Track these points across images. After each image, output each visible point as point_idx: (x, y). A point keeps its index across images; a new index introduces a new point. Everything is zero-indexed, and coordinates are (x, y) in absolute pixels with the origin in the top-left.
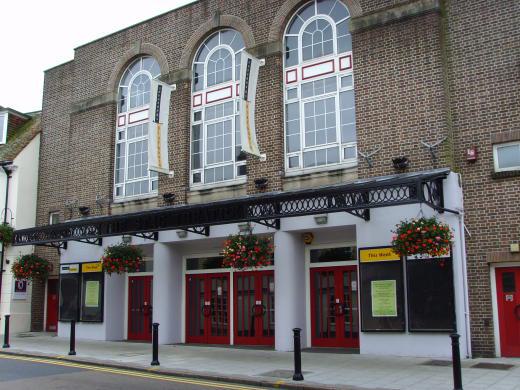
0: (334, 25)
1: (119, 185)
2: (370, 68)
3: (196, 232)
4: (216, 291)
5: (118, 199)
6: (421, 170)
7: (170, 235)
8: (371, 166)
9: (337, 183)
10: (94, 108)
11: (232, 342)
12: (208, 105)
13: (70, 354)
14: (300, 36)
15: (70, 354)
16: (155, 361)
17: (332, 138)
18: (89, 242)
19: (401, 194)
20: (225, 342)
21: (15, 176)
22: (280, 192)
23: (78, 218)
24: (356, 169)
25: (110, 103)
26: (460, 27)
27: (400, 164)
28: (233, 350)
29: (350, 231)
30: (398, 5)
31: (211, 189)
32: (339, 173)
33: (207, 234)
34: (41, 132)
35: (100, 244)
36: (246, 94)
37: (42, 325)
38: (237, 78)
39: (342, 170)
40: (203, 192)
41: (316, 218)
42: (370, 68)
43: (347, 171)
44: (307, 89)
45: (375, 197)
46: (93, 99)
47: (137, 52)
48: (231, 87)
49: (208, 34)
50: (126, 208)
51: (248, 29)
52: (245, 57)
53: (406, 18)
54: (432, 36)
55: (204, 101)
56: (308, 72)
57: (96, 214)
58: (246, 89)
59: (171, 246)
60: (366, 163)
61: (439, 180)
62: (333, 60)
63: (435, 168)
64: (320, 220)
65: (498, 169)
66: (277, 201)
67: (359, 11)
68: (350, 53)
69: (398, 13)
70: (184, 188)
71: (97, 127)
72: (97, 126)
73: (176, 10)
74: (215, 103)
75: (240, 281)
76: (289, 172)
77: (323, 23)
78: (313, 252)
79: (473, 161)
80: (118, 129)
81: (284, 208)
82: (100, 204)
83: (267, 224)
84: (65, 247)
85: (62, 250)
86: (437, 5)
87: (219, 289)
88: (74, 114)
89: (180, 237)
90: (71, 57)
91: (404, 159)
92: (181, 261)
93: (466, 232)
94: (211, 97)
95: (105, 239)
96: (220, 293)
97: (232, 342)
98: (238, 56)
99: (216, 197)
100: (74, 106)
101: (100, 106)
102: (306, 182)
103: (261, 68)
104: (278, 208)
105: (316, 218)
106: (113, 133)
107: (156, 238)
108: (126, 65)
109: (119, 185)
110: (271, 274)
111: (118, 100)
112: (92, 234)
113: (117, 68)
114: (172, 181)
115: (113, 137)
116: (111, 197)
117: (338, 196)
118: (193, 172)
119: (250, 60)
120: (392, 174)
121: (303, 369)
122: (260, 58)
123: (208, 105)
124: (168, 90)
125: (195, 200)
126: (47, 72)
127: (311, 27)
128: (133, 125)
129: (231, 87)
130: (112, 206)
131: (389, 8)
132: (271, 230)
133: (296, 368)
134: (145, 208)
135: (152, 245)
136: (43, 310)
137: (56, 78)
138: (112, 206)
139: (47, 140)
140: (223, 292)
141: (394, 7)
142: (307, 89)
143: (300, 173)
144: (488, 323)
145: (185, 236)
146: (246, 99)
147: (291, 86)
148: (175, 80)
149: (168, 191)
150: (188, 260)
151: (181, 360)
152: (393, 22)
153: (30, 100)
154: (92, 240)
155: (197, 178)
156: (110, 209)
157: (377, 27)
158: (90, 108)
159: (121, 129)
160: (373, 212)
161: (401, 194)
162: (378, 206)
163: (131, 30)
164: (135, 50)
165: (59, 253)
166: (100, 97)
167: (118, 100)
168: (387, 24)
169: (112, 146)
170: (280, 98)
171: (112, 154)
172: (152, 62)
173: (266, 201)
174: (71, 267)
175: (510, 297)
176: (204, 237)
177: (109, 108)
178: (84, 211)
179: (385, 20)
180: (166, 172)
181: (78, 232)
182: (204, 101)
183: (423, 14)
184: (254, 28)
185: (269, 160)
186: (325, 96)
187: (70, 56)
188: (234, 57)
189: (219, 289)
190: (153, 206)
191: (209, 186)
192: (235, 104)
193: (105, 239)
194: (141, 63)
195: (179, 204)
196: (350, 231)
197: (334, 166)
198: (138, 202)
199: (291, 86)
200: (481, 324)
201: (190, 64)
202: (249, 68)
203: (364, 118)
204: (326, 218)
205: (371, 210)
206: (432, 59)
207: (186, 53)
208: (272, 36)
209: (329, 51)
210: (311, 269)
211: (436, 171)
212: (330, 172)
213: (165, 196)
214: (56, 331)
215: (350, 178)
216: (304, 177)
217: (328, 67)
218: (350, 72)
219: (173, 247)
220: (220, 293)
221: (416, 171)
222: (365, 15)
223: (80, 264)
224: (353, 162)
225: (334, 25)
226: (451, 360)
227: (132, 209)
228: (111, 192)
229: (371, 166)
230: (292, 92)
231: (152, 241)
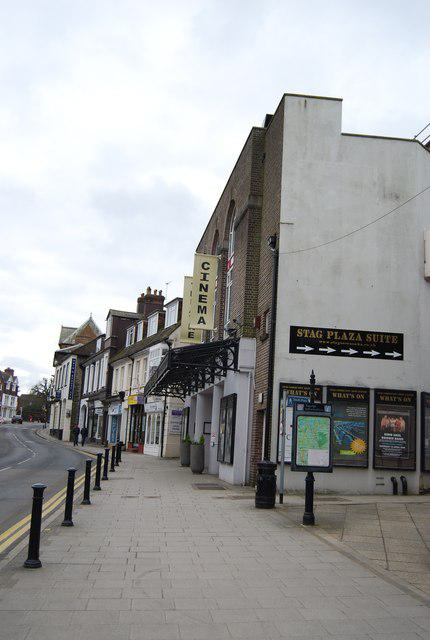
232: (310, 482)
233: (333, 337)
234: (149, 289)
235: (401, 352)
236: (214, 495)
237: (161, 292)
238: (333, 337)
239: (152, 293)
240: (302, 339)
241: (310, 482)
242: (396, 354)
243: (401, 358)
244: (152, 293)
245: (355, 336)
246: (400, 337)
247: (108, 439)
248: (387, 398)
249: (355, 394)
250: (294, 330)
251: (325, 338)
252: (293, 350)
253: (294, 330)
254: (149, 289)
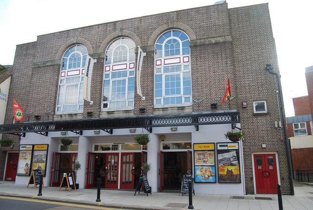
0: (181, 42)
2: (199, 63)
4: (111, 162)
5: (57, 113)
7: (90, 133)
10: (48, 66)
11: (119, 188)
12: (113, 71)
13: (39, 195)
14: (68, 58)
15: (39, 195)
16: (40, 194)
17: (179, 92)
18: (41, 134)
19: (189, 121)
20: (115, 187)
22: (152, 115)
24: (191, 107)
25: (57, 65)
28: (119, 191)
29: (189, 135)
30: (214, 37)
31: (130, 110)
32: (183, 108)
33: (112, 133)
34: (12, 75)
35: (47, 135)
36: (87, 74)
37: (3, 177)
38: (84, 65)
39: (184, 107)
40: (109, 113)
41: (95, 132)
42: (199, 63)
44: (114, 75)
45: (154, 122)
46: (47, 62)
49: (115, 38)
52: (88, 57)
53: (217, 43)
54: (228, 52)
55: (111, 70)
56: (167, 62)
57: (44, 120)
58: (88, 72)
60: (196, 105)
62: (126, 64)
63: (230, 109)
64: (173, 129)
66: (151, 119)
67: (194, 37)
68: (189, 55)
69: (213, 41)
70: (99, 110)
71: (48, 76)
72: (49, 75)
73: (98, 25)
74: (71, 77)
75: (124, 157)
76: (156, 106)
77: (175, 41)
79: (245, 108)
80: (60, 78)
81: (50, 128)
82: (48, 115)
83: (76, 133)
84: (24, 136)
85: (22, 137)
86: (231, 40)
87: (113, 161)
88: (35, 68)
90: (35, 39)
91: (216, 104)
92: (58, 145)
94: (70, 74)
95: (114, 130)
96: (113, 163)
97: (119, 188)
98: (84, 59)
99: (116, 116)
100: (35, 64)
101: (50, 66)
102: (166, 112)
103: (95, 63)
104: (48, 127)
105: (95, 132)
106: (58, 80)
107: (81, 134)
111: (61, 64)
112: (43, 130)
113: (62, 48)
114: (92, 106)
116: (54, 111)
117: (180, 116)
118: (103, 103)
119: (90, 59)
121: (193, 204)
122: (94, 59)
123: (113, 71)
124: (93, 61)
125: (104, 116)
127: (169, 41)
128: (115, 71)
130: (54, 116)
131: (208, 38)
132: (78, 135)
133: (98, 197)
134: (74, 118)
135: (78, 137)
136: (4, 169)
137: (23, 50)
138: (54, 116)
139: (15, 80)
140: (115, 162)
141: (211, 38)
142: (114, 75)
143: (162, 107)
144: (252, 179)
146: (87, 76)
147: (107, 73)
149: (142, 107)
151: (89, 196)
152: (211, 44)
153: (7, 59)
154: (43, 133)
155: (105, 106)
157: (203, 45)
158: (45, 66)
159: (62, 78)
160: (200, 126)
161: (189, 121)
162: (204, 124)
163: (97, 27)
166: (52, 61)
167: (61, 64)
168: (208, 45)
169: (57, 86)
170: (153, 72)
174: (27, 146)
175: (260, 167)
176: (109, 134)
177: (56, 67)
178: (37, 117)
179: (207, 43)
180: (90, 101)
182: (111, 70)
183: (224, 43)
184: (86, 46)
185: (146, 100)
186: (122, 78)
188: (82, 57)
189: (113, 161)
190: (80, 118)
191: (166, 106)
192: (81, 78)
193: (114, 130)
194: (76, 47)
195: (95, 118)
196: (189, 135)
197: (179, 105)
198: (71, 115)
199: (159, 67)
200: (249, 179)
202: (89, 63)
203: (196, 84)
204: (135, 130)
205: (199, 126)
206: (229, 62)
208: (150, 43)
209: (178, 52)
213: (88, 113)
214: (50, 186)
216: (164, 109)
217: (177, 60)
218: (189, 63)
219: (90, 139)
220: (113, 163)
222: (197, 40)
223: (33, 146)
224: (190, 103)
225: (181, 42)
227: (68, 119)
229: (199, 106)
230: (107, 76)
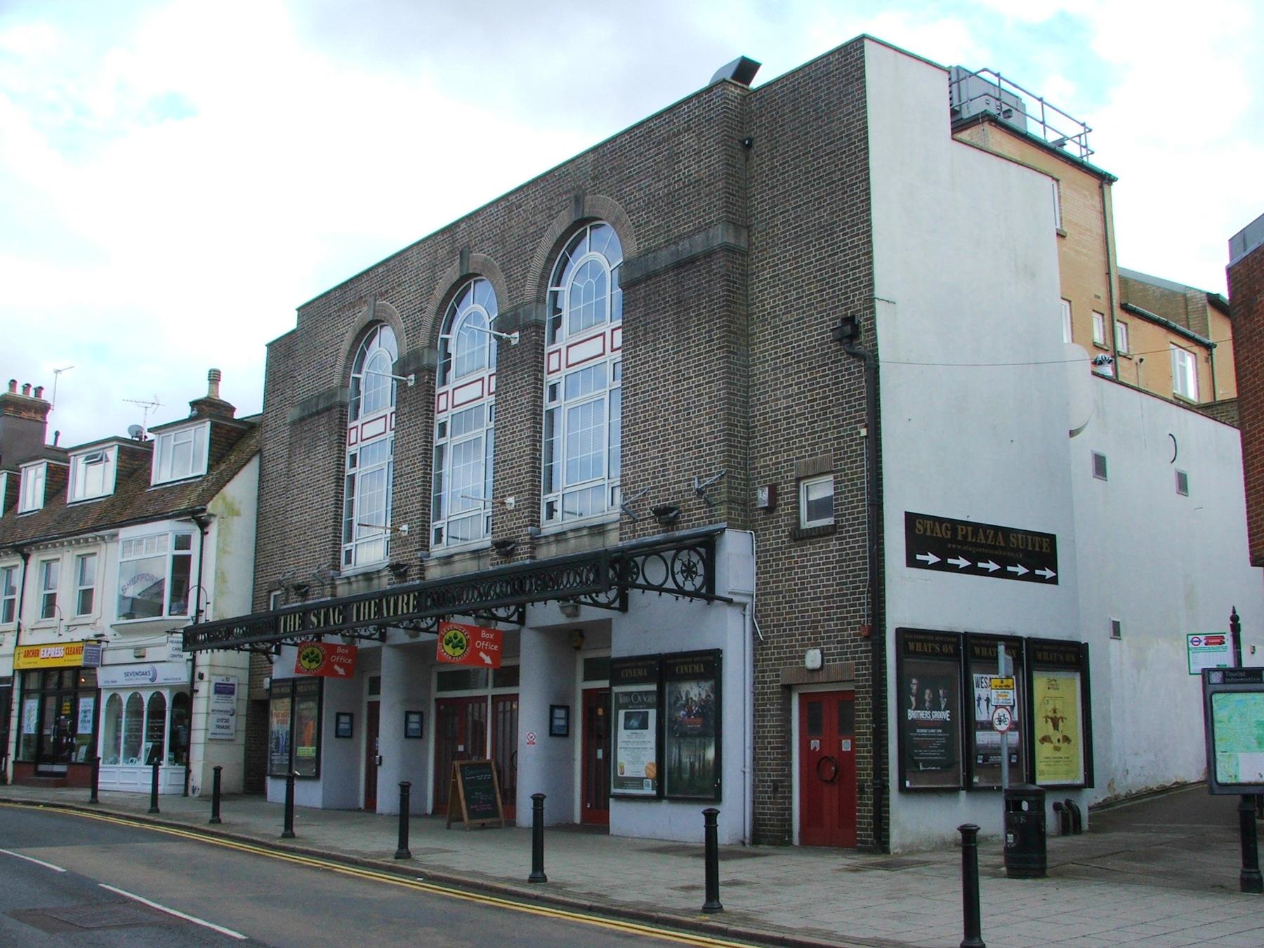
1: (438, 524)
3: (596, 604)
6: (693, 526)
7: (547, 613)
8: (635, 521)
9: (596, 545)
13: (212, 822)
21: (213, 529)
23: (653, 534)
26: (767, 274)
27: (666, 516)
43: (456, 558)
47: (370, 318)
48: (603, 334)
49: (455, 286)
50: (355, 586)
51: (501, 277)
59: (550, 633)
60: (630, 514)
61: (708, 545)
65: (806, 524)
78: (588, 662)
84: (278, 652)
89: (568, 616)
93: (755, 633)
106: (538, 389)
107: (522, 620)
108: (357, 340)
109: (438, 524)
110: (515, 697)
115: (340, 465)
120: (659, 533)
126: (271, 346)
129: (603, 334)
135: (379, 649)
137: (282, 354)
145: (576, 613)
148: (412, 368)
150: (439, 674)
156: (334, 587)
164: (364, 314)
165: (271, 663)
169: (339, 480)
171: (536, 432)
172: (608, 233)
173: (517, 577)
175: (815, 744)
178: (302, 590)
181: (655, 572)
184: (508, 276)
187: (289, 323)
195: (522, 559)
196: (604, 628)
200: (767, 787)
201: (345, 376)
206: (717, 334)
207: (428, 319)
210: (585, 692)
211: (711, 527)
212: (590, 528)
215: (613, 540)
221: (688, 527)
224: (615, 513)
226: (411, 820)
228: (336, 558)
229: (635, 521)
231: (377, 643)
232: (289, 833)
233: (965, 536)
234: (13, 383)
235: (1054, 569)
236: (836, 867)
237: (39, 390)
238: (965, 536)
239: (19, 391)
240: (942, 542)
241: (289, 833)
242: (1048, 573)
243: (1054, 581)
244: (19, 391)
245: (996, 536)
246: (1052, 538)
247: (100, 753)
248: (919, 649)
249: (942, 643)
250: (911, 518)
251: (954, 539)
252: (912, 562)
253: (911, 518)
254: (13, 383)
